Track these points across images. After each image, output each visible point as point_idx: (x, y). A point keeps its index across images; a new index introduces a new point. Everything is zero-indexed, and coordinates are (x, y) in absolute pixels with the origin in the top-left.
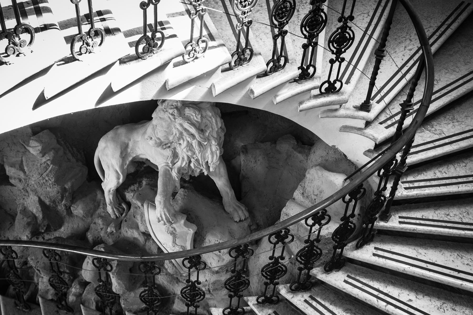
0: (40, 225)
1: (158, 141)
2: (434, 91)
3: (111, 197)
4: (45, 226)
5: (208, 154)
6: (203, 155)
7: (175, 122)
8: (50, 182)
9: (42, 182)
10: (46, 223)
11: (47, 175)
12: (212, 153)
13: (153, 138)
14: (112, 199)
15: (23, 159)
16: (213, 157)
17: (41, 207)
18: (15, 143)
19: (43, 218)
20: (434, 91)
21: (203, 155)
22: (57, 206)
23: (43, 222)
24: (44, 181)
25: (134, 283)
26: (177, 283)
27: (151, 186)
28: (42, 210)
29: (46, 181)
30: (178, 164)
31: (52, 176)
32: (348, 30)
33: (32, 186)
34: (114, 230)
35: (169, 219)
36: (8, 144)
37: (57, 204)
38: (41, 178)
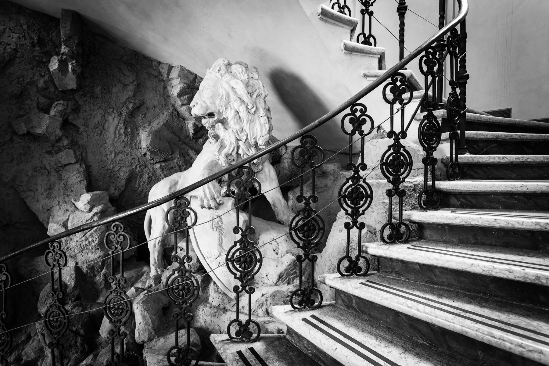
0: (68, 295)
1: (204, 105)
2: (459, 24)
3: (156, 254)
4: (74, 296)
5: (257, 126)
6: (251, 127)
7: (222, 80)
8: (93, 244)
9: (84, 243)
10: (76, 293)
11: (91, 235)
12: (261, 125)
13: (199, 103)
14: (156, 258)
15: (70, 218)
16: (262, 130)
17: (76, 274)
18: (65, 202)
19: (75, 286)
20: (459, 24)
21: (251, 127)
22: (95, 276)
23: (73, 292)
24: (87, 242)
25: (166, 327)
26: (224, 313)
27: (198, 272)
28: (76, 277)
29: (89, 242)
30: (225, 151)
31: (96, 237)
32: (350, 210)
33: (73, 249)
34: (153, 283)
35: (214, 195)
36: (59, 202)
37: (96, 272)
38: (84, 238)
